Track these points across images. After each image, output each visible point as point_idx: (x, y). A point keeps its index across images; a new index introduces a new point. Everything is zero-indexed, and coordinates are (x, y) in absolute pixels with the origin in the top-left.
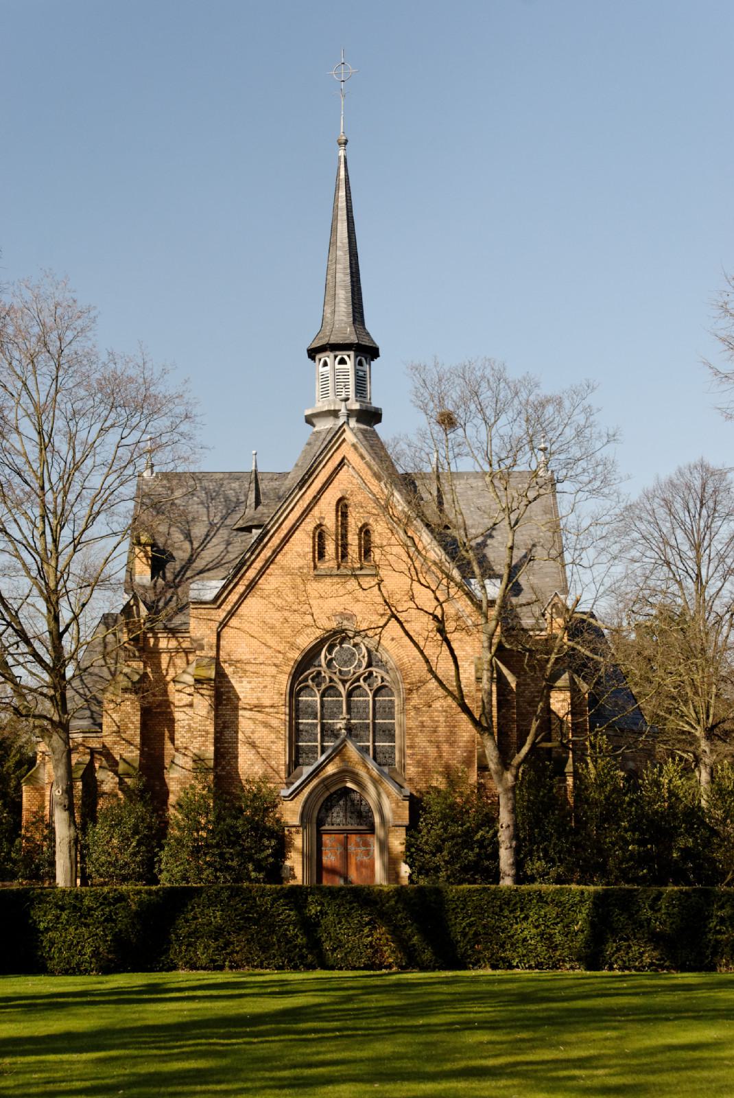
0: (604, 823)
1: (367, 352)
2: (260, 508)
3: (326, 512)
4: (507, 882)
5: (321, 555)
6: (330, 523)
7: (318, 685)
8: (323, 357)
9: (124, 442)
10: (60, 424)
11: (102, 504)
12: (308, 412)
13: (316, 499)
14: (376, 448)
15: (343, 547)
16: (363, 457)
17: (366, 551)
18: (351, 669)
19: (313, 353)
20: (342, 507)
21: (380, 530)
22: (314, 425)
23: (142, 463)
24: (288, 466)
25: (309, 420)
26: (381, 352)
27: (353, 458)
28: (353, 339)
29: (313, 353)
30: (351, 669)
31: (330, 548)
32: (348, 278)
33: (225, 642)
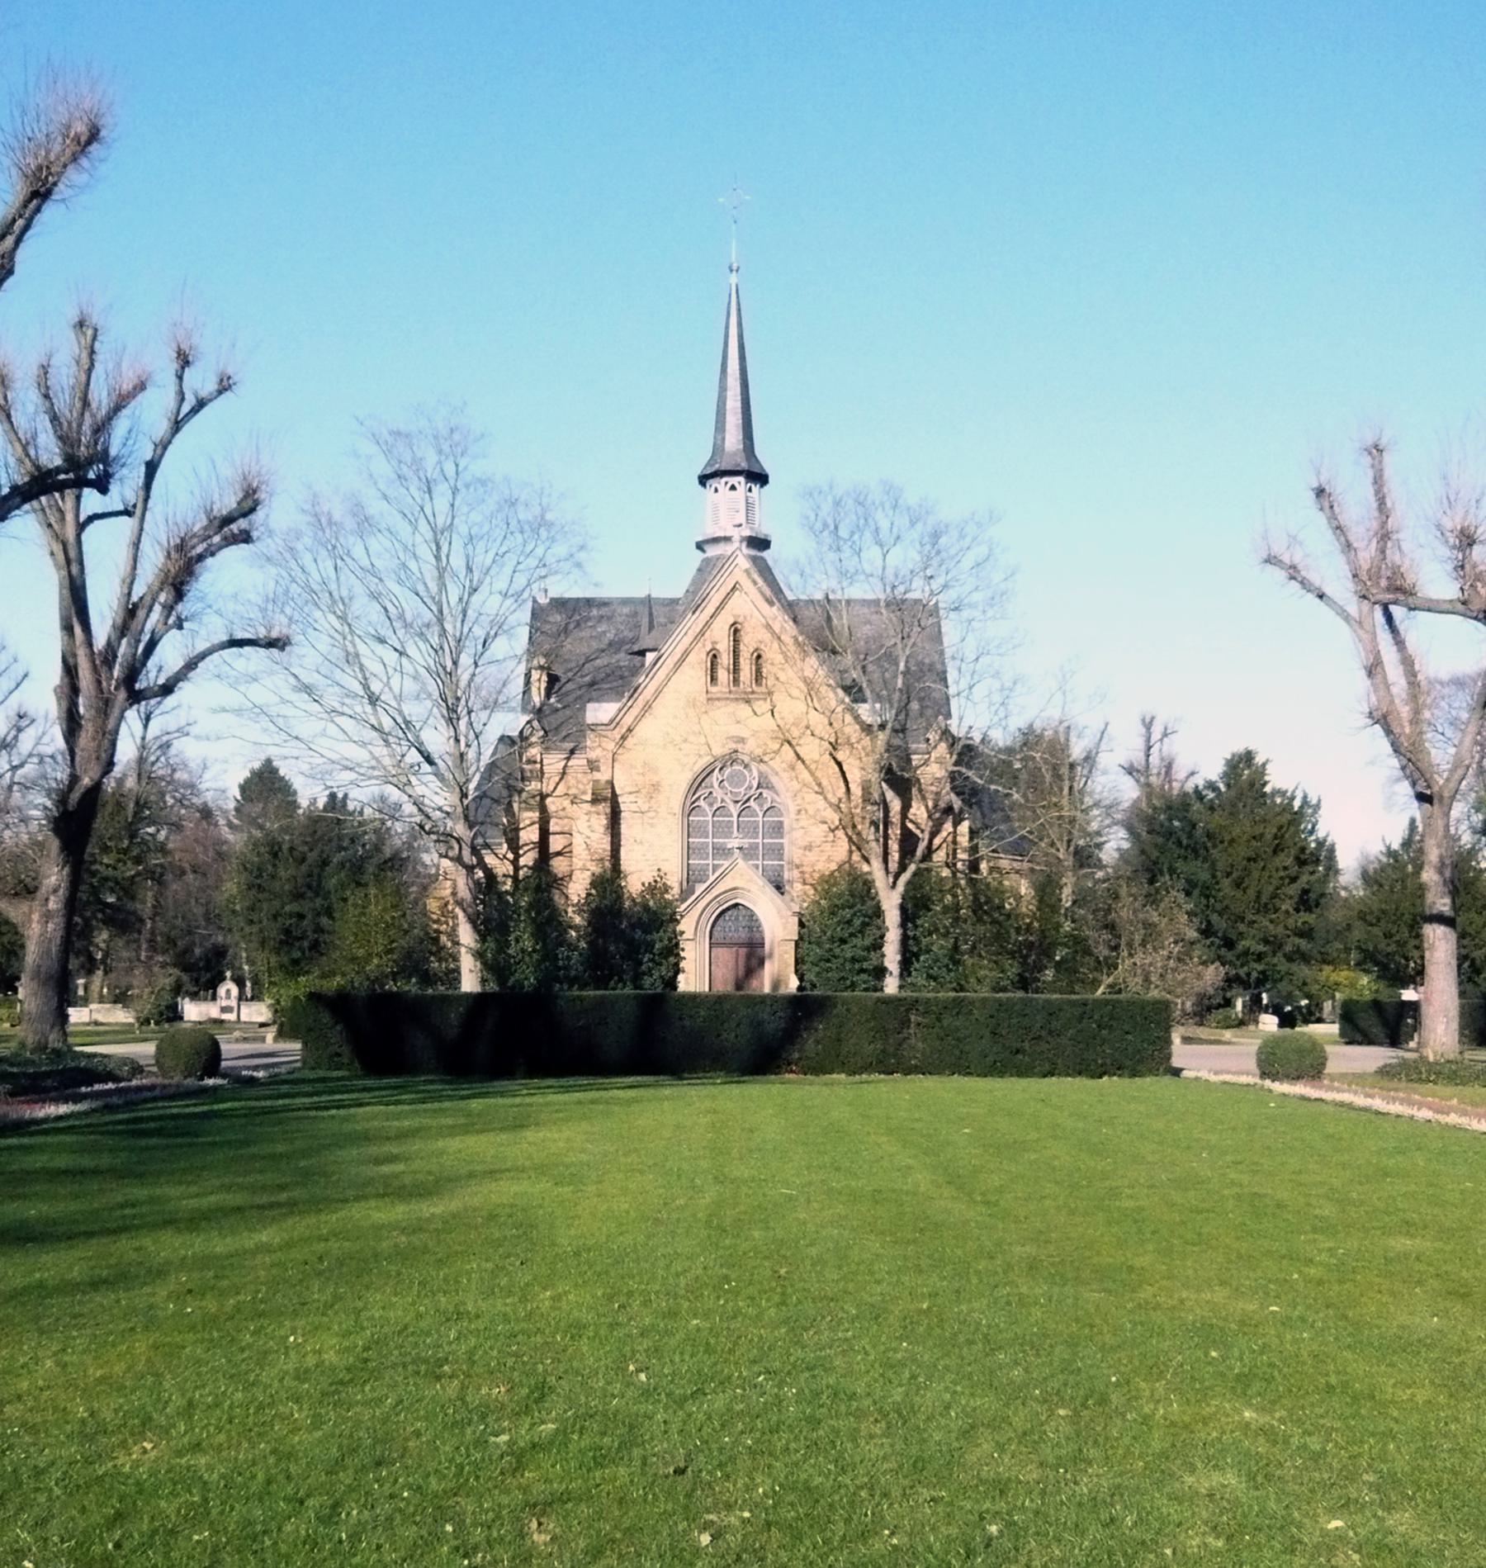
0: (1308, 1006)
1: (759, 478)
2: (654, 633)
3: (720, 635)
4: (891, 986)
5: (714, 679)
6: (724, 647)
7: (711, 805)
8: (714, 483)
9: (520, 567)
10: (457, 544)
11: (498, 628)
12: (700, 539)
13: (707, 625)
14: (765, 571)
15: (736, 669)
16: (755, 583)
17: (758, 677)
18: (742, 790)
19: (703, 480)
20: (736, 632)
21: (772, 654)
22: (703, 551)
23: (535, 586)
24: (678, 593)
25: (700, 546)
26: (770, 479)
27: (746, 583)
28: (744, 465)
29: (703, 480)
30: (742, 790)
31: (722, 675)
32: (739, 404)
33: (59, 776)
